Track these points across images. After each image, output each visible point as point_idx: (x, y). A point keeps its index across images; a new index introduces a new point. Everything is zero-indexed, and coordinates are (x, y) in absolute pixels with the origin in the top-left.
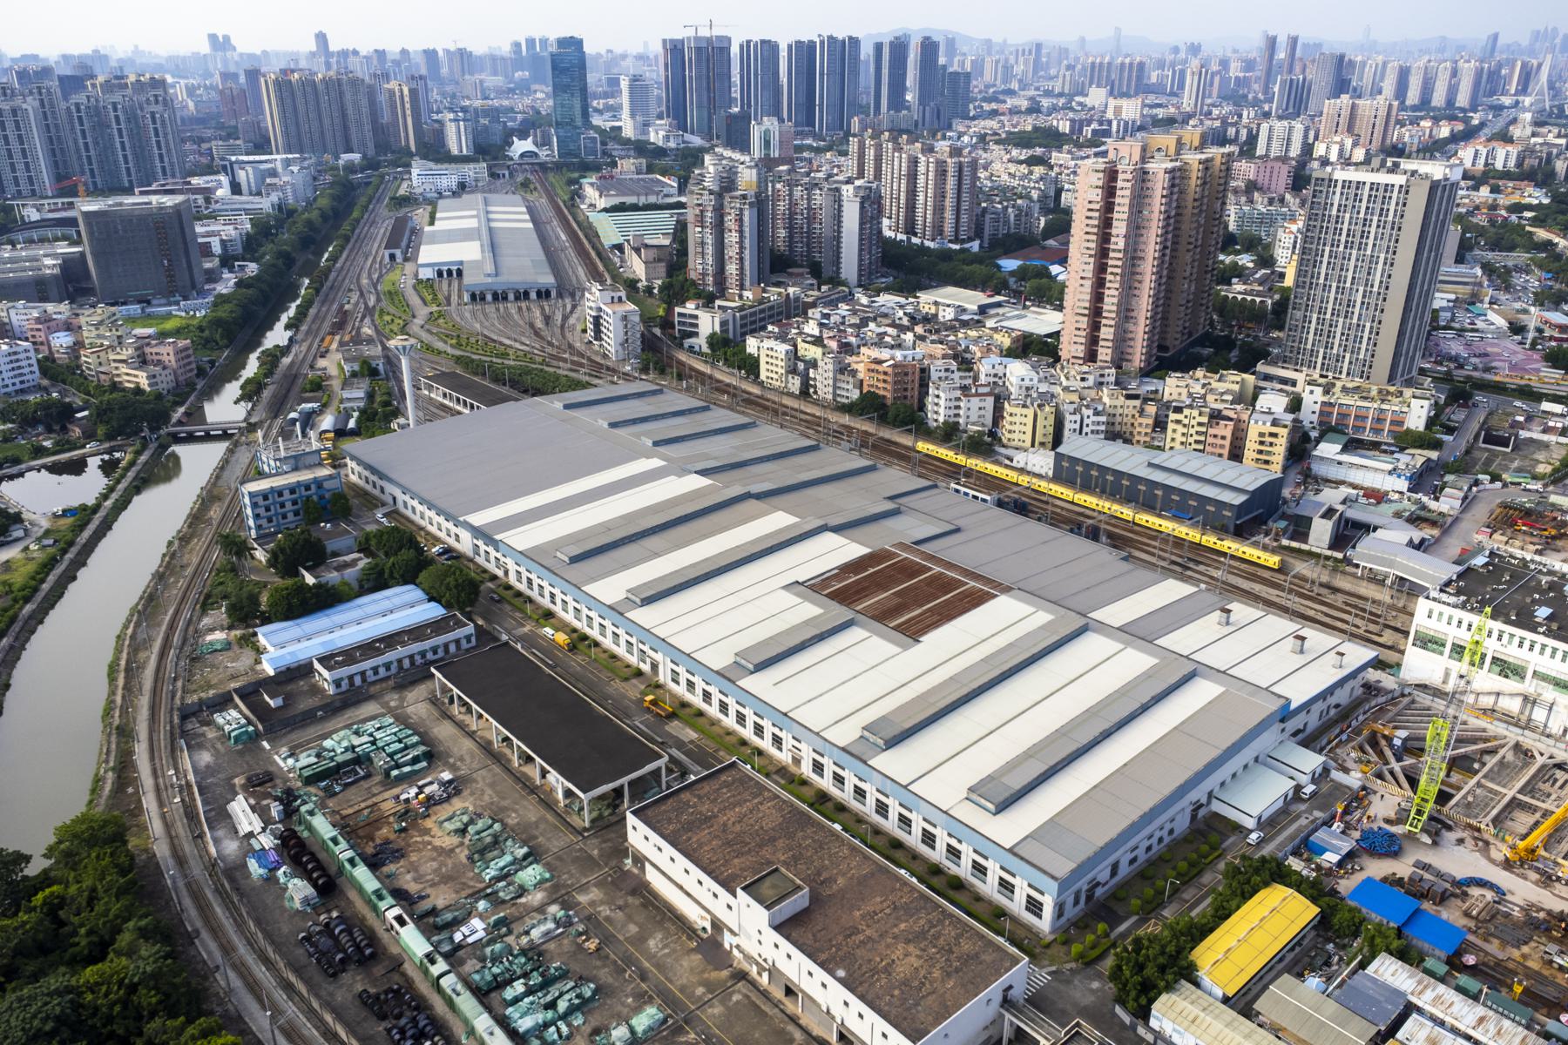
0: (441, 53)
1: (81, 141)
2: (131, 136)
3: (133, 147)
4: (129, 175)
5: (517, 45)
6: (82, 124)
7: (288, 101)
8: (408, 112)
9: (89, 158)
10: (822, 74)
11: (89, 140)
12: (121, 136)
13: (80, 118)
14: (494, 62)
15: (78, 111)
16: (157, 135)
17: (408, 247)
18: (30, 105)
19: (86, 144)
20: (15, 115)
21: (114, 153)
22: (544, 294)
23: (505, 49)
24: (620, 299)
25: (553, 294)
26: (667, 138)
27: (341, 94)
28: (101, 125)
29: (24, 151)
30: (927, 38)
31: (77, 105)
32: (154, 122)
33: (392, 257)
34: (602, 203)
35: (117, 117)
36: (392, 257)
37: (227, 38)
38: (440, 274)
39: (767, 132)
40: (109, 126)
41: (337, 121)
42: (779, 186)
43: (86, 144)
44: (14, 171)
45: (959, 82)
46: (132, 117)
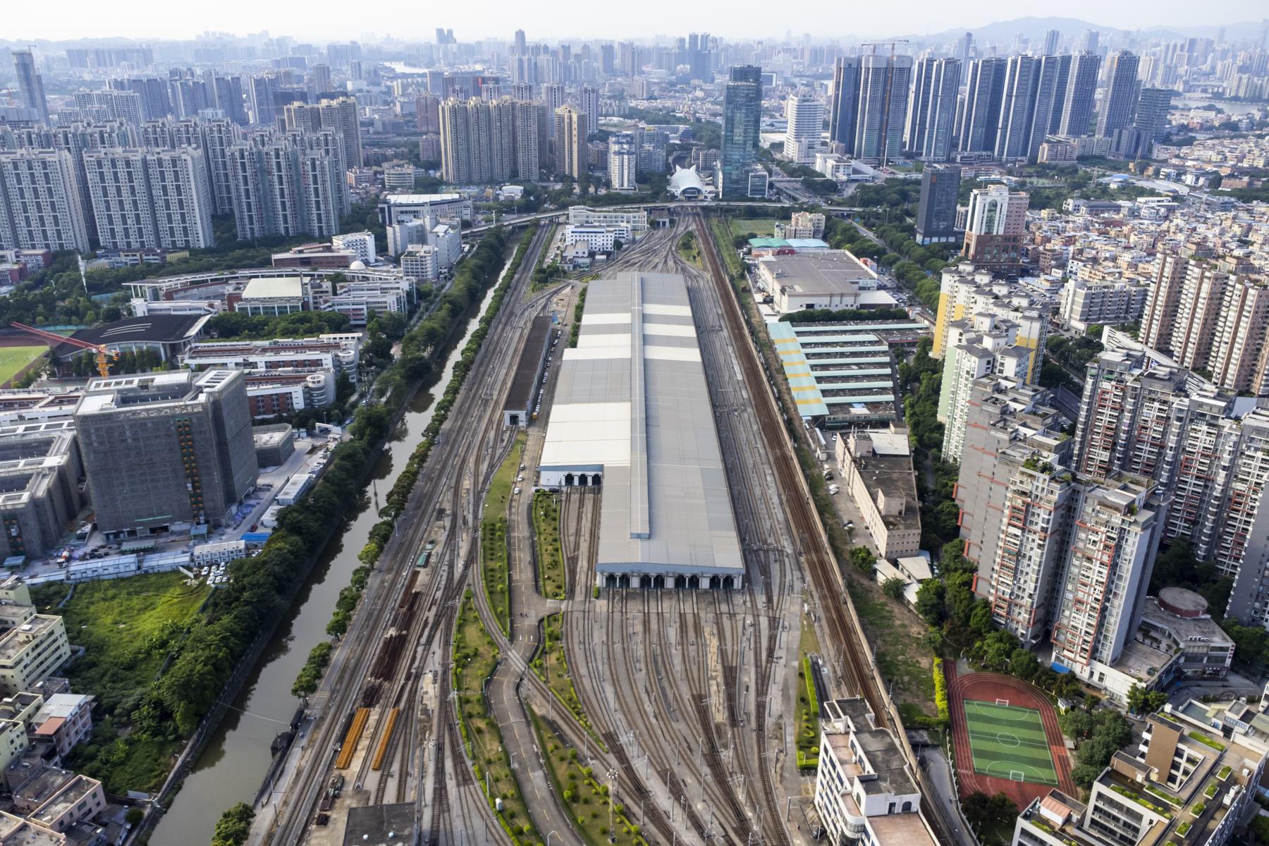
0: (616, 46)
1: (242, 188)
2: (290, 182)
3: (292, 194)
4: (286, 222)
5: (682, 41)
6: (244, 170)
7: (462, 127)
8: (575, 139)
9: (249, 204)
10: (1009, 96)
11: (251, 186)
12: (281, 183)
13: (243, 165)
14: (661, 55)
15: (242, 157)
16: (315, 182)
17: (535, 404)
18: (191, 155)
19: (247, 191)
20: (175, 165)
21: (273, 201)
22: (722, 583)
23: (672, 45)
24: (907, 806)
25: (737, 584)
26: (837, 168)
27: (514, 118)
28: (262, 171)
29: (181, 201)
30: (1125, 53)
31: (242, 152)
32: (314, 169)
33: (514, 419)
34: (785, 305)
35: (279, 164)
36: (514, 419)
37: (450, 32)
38: (569, 479)
39: (994, 204)
40: (270, 173)
41: (505, 141)
42: (1106, 385)
43: (247, 191)
44: (170, 221)
45: (1161, 100)
46: (294, 164)
